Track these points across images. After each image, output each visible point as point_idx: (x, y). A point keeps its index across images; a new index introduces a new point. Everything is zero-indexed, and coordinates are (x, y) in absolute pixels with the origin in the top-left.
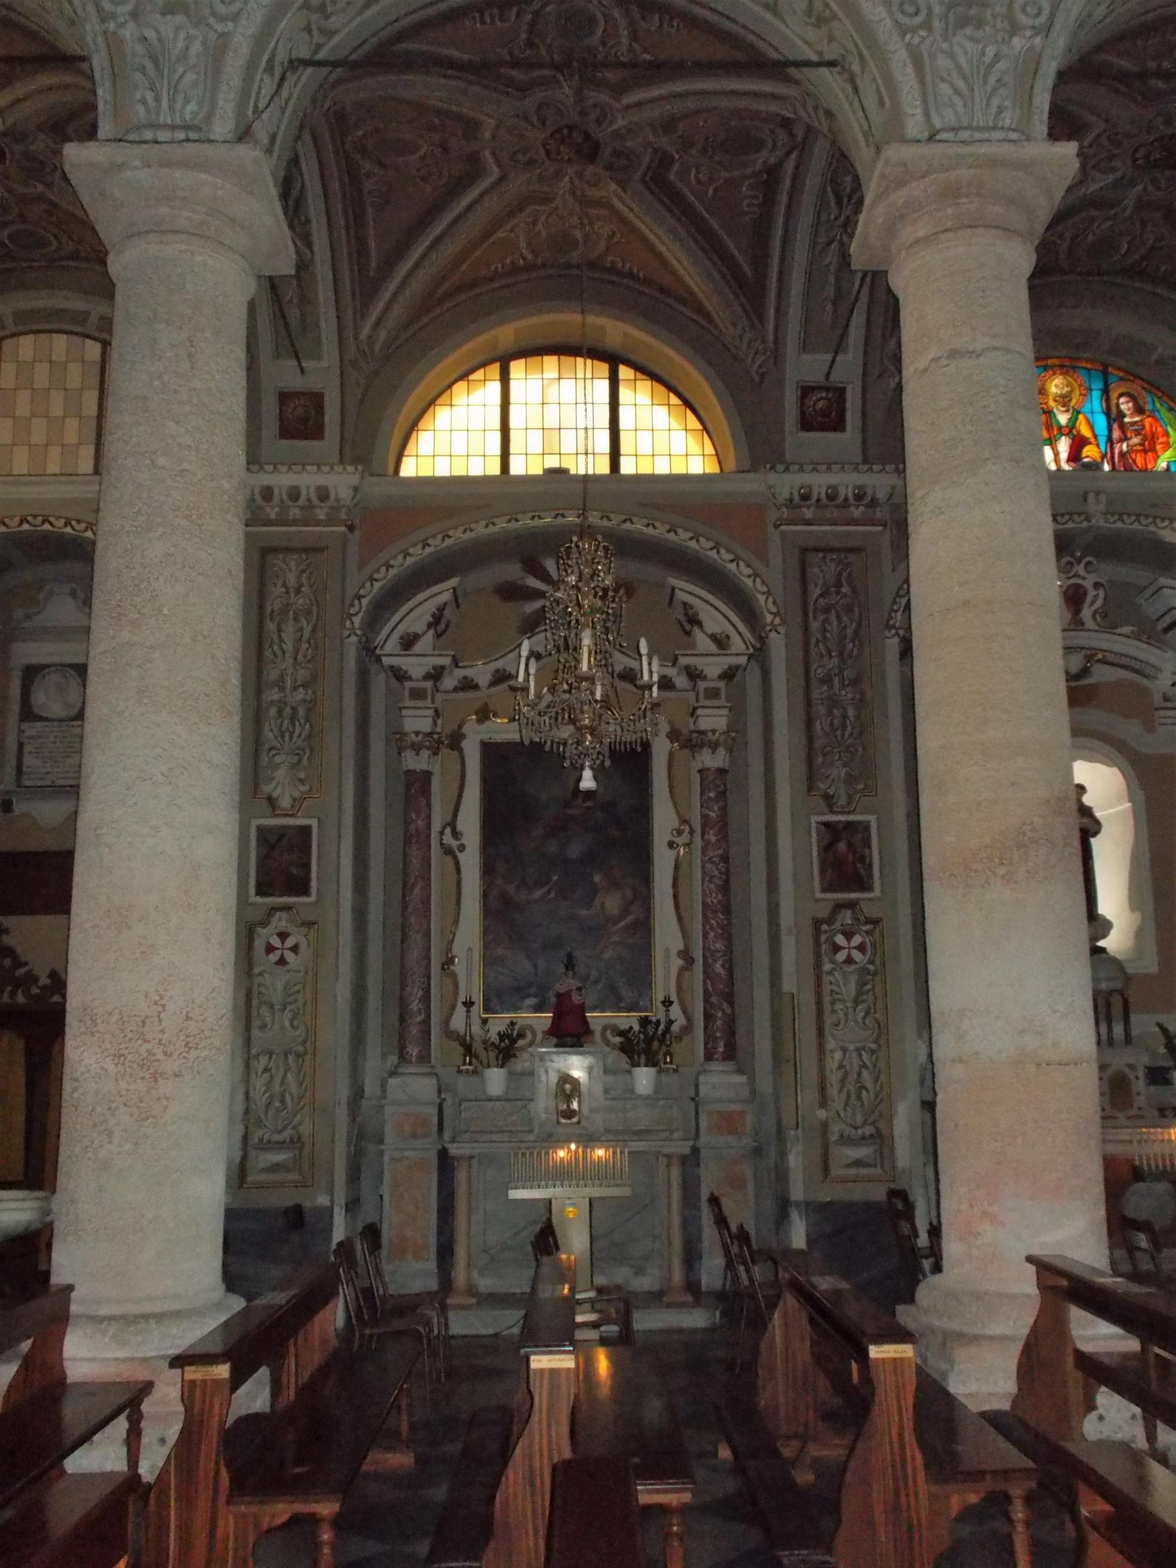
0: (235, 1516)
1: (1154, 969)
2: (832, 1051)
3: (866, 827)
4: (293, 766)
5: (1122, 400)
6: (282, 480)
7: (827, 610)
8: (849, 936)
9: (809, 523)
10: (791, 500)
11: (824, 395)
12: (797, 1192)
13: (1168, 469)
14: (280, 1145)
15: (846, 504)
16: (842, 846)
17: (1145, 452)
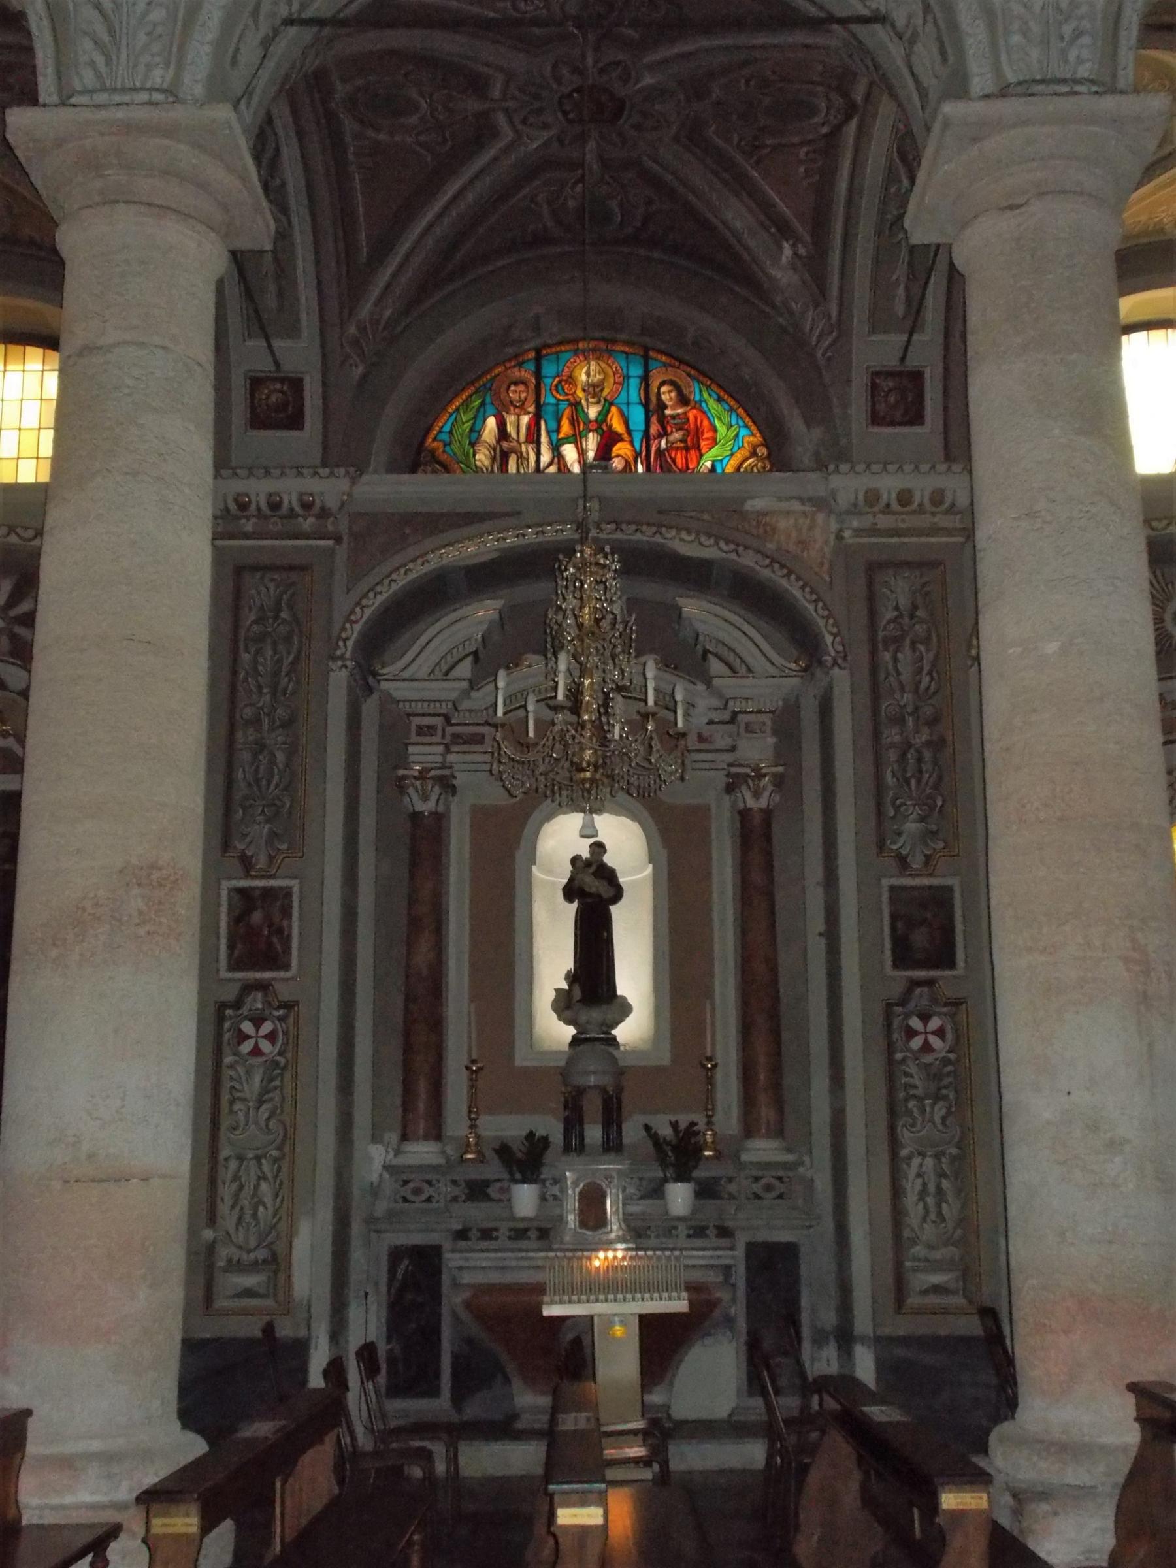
0: (749, 1131)
1: (518, 1062)
2: (226, 1159)
3: (287, 893)
4: (922, 819)
5: (664, 389)
6: (258, 489)
7: (261, 638)
8: (925, 1018)
9: (247, 536)
10: (855, 505)
11: (278, 386)
12: (863, 1323)
13: (713, 469)
14: (254, 1267)
15: (292, 514)
16: (257, 917)
17: (687, 449)
